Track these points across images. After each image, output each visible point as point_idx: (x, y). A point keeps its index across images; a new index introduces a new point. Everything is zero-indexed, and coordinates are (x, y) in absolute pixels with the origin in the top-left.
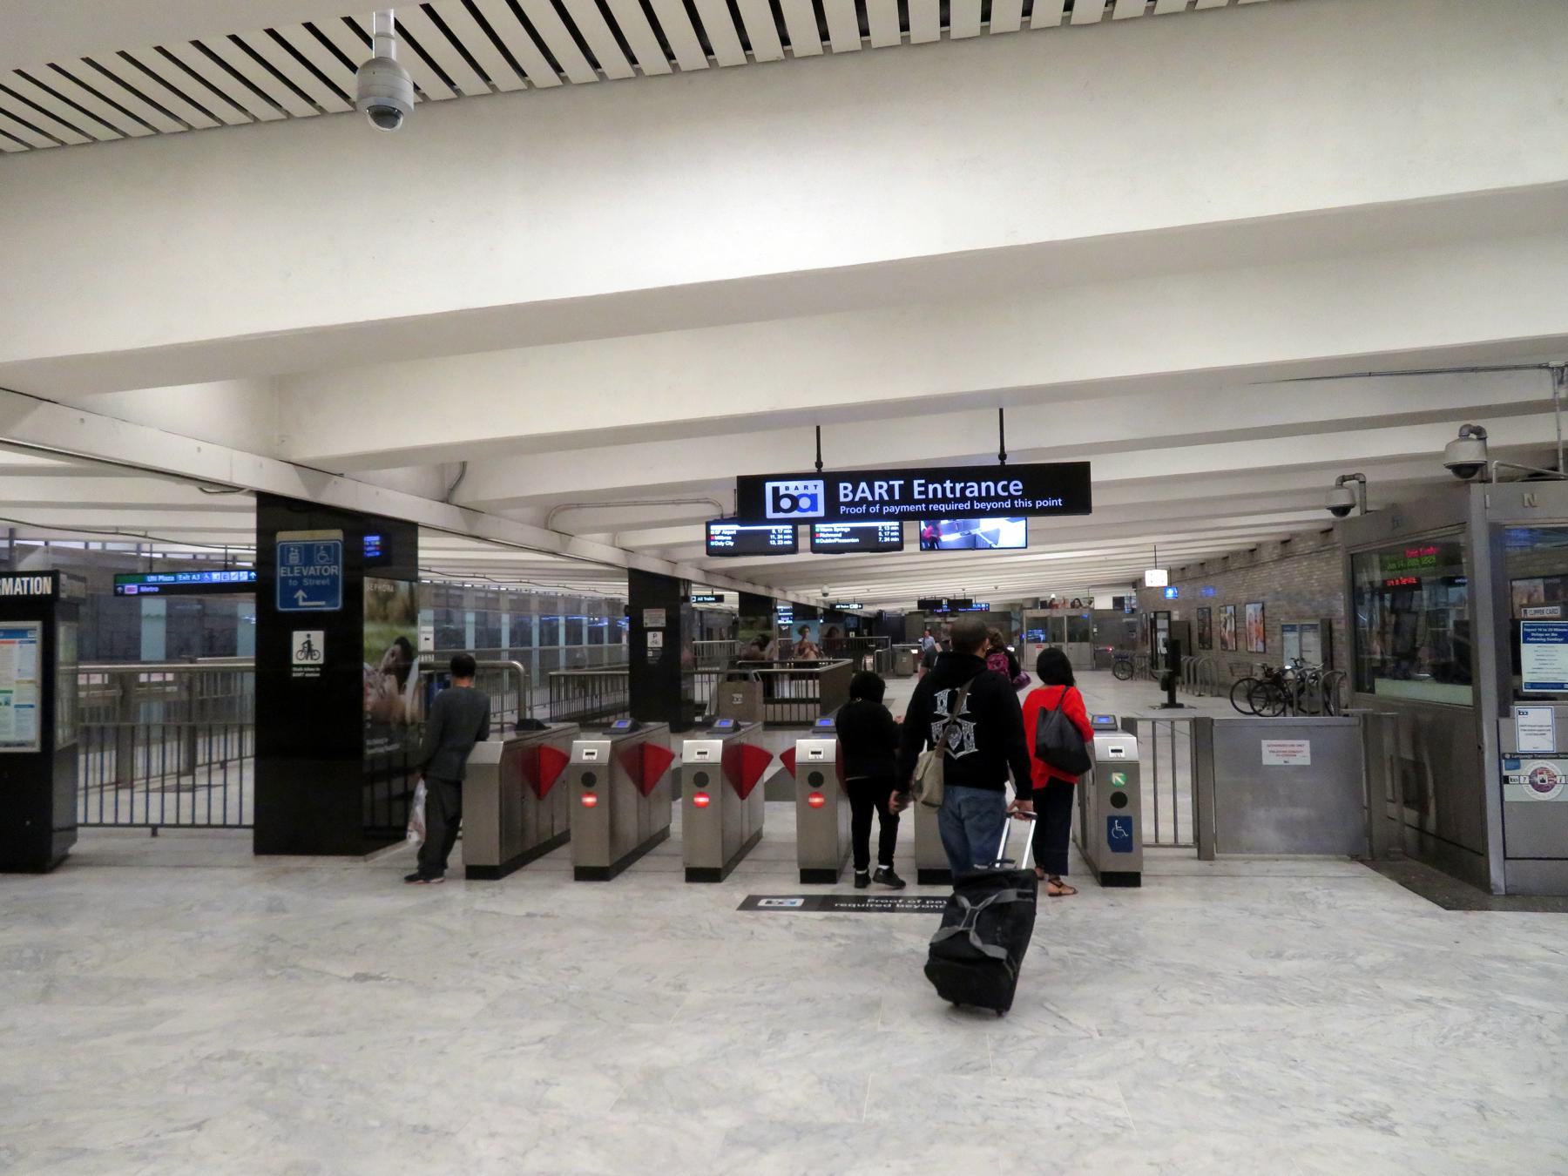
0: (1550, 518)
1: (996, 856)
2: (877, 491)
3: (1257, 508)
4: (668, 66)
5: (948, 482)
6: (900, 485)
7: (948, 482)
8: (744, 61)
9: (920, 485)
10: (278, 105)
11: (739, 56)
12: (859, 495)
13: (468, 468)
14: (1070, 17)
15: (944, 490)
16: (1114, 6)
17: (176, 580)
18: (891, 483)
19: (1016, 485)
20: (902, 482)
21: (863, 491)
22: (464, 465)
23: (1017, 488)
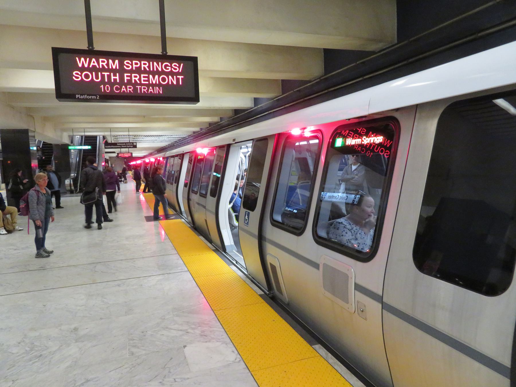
0: (42, 267)
1: (292, 93)
2: (101, 63)
6: (182, 78)
9: (127, 76)
12: (92, 64)
13: (28, 234)
15: (83, 97)
17: (363, 78)
20: (183, 77)
21: (94, 62)
22: (29, 234)
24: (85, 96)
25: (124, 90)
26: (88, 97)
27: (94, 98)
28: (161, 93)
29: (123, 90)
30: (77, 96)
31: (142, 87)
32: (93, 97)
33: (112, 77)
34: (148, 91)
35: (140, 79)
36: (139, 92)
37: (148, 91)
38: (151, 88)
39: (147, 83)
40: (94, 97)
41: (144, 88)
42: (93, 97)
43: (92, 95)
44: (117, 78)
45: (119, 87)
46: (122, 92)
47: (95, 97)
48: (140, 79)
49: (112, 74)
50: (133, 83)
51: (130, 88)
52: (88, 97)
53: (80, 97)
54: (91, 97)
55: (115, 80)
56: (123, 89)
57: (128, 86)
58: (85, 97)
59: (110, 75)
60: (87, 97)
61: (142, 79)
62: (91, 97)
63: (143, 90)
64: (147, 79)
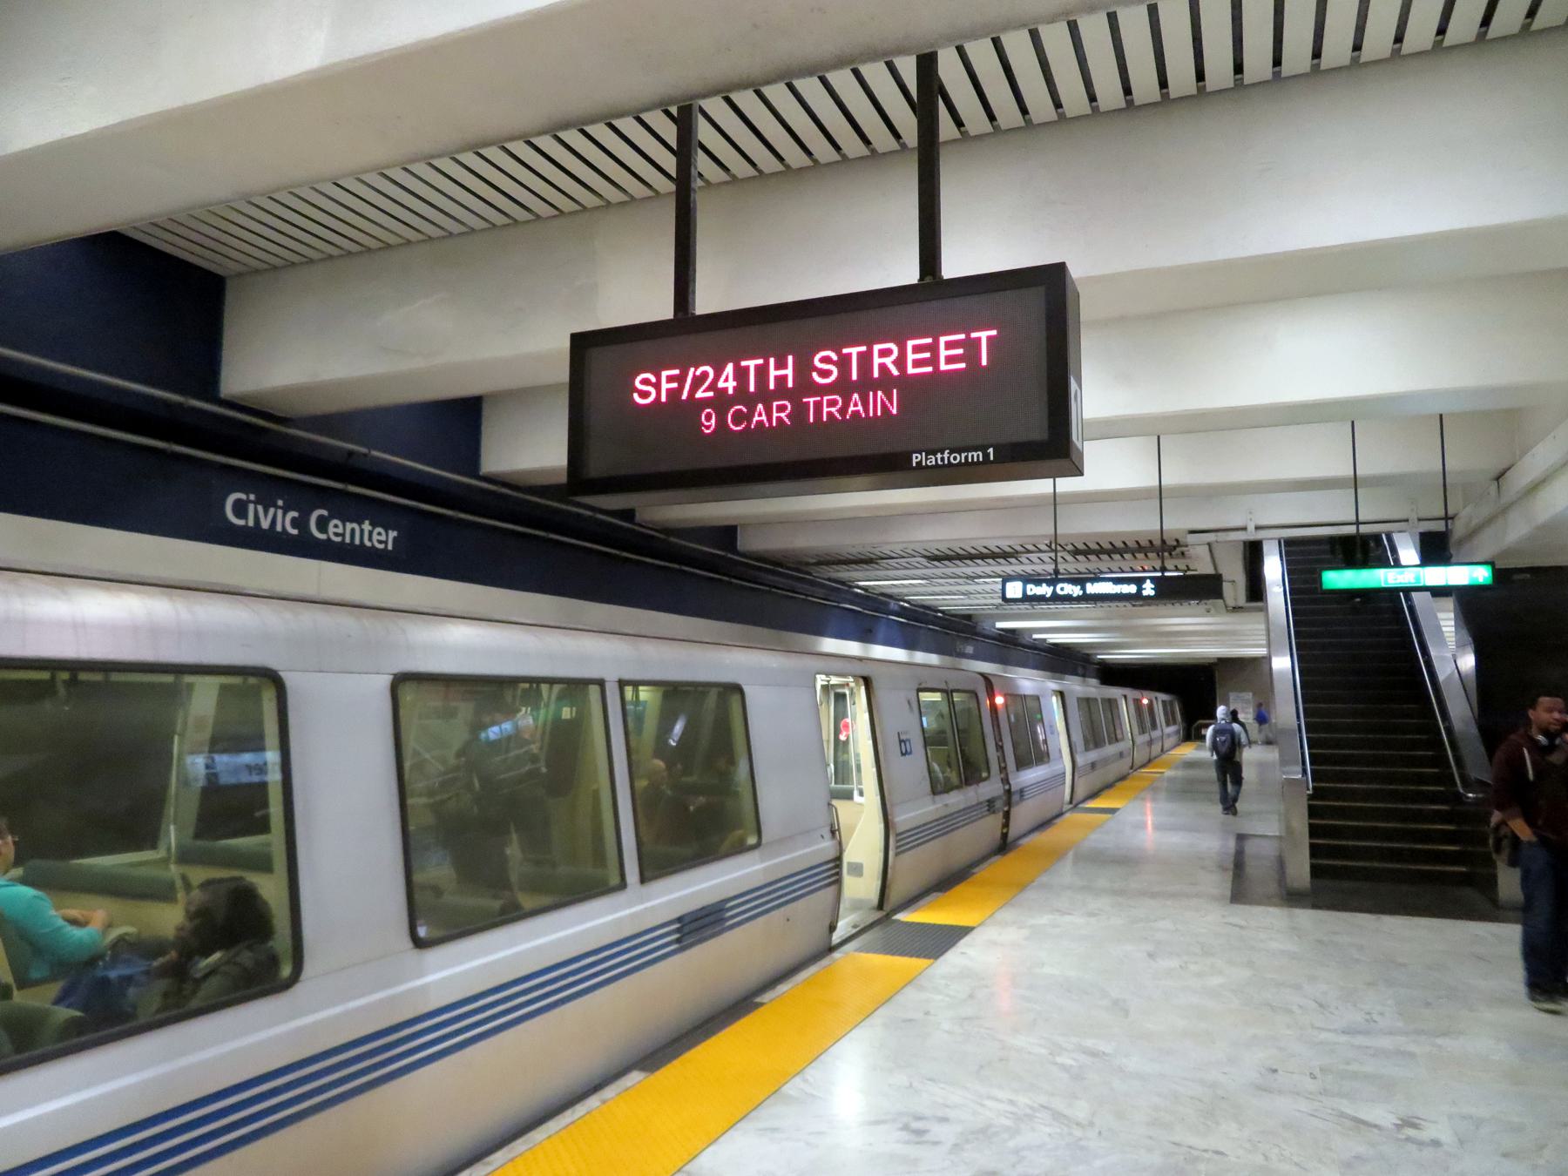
3: (1074, 738)
4: (1055, 113)
5: (367, 522)
6: (989, 338)
7: (367, 522)
8: (1023, 124)
10: (624, 190)
11: (986, 126)
14: (1400, 49)
15: (936, 459)
16: (1533, 19)
18: (845, 351)
19: (379, 534)
20: (994, 333)
22: (1441, 416)
23: (336, 530)
24: (943, 453)
25: (855, 409)
26: (955, 458)
27: (975, 460)
28: (895, 411)
29: (756, 418)
30: (915, 460)
31: (822, 399)
32: (973, 456)
33: (773, 373)
34: (843, 411)
35: (901, 362)
36: (811, 420)
37: (843, 411)
38: (858, 399)
39: (930, 369)
40: (977, 456)
41: (832, 403)
42: (973, 456)
43: (968, 450)
44: (789, 372)
45: (745, 410)
46: (753, 427)
47: (980, 453)
48: (901, 362)
49: (772, 361)
50: (663, 403)
51: (781, 409)
52: (955, 458)
53: (927, 459)
54: (966, 457)
55: (781, 380)
56: (855, 406)
57: (775, 404)
58: (942, 459)
59: (767, 363)
60: (949, 458)
61: (911, 357)
62: (963, 455)
63: (825, 410)
64: (927, 355)
